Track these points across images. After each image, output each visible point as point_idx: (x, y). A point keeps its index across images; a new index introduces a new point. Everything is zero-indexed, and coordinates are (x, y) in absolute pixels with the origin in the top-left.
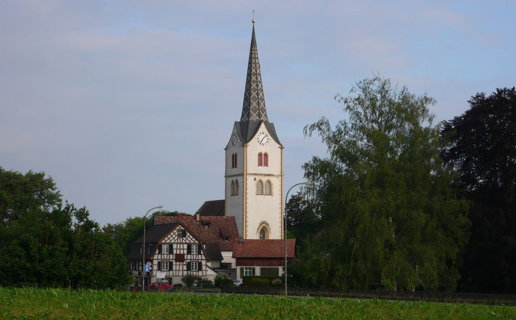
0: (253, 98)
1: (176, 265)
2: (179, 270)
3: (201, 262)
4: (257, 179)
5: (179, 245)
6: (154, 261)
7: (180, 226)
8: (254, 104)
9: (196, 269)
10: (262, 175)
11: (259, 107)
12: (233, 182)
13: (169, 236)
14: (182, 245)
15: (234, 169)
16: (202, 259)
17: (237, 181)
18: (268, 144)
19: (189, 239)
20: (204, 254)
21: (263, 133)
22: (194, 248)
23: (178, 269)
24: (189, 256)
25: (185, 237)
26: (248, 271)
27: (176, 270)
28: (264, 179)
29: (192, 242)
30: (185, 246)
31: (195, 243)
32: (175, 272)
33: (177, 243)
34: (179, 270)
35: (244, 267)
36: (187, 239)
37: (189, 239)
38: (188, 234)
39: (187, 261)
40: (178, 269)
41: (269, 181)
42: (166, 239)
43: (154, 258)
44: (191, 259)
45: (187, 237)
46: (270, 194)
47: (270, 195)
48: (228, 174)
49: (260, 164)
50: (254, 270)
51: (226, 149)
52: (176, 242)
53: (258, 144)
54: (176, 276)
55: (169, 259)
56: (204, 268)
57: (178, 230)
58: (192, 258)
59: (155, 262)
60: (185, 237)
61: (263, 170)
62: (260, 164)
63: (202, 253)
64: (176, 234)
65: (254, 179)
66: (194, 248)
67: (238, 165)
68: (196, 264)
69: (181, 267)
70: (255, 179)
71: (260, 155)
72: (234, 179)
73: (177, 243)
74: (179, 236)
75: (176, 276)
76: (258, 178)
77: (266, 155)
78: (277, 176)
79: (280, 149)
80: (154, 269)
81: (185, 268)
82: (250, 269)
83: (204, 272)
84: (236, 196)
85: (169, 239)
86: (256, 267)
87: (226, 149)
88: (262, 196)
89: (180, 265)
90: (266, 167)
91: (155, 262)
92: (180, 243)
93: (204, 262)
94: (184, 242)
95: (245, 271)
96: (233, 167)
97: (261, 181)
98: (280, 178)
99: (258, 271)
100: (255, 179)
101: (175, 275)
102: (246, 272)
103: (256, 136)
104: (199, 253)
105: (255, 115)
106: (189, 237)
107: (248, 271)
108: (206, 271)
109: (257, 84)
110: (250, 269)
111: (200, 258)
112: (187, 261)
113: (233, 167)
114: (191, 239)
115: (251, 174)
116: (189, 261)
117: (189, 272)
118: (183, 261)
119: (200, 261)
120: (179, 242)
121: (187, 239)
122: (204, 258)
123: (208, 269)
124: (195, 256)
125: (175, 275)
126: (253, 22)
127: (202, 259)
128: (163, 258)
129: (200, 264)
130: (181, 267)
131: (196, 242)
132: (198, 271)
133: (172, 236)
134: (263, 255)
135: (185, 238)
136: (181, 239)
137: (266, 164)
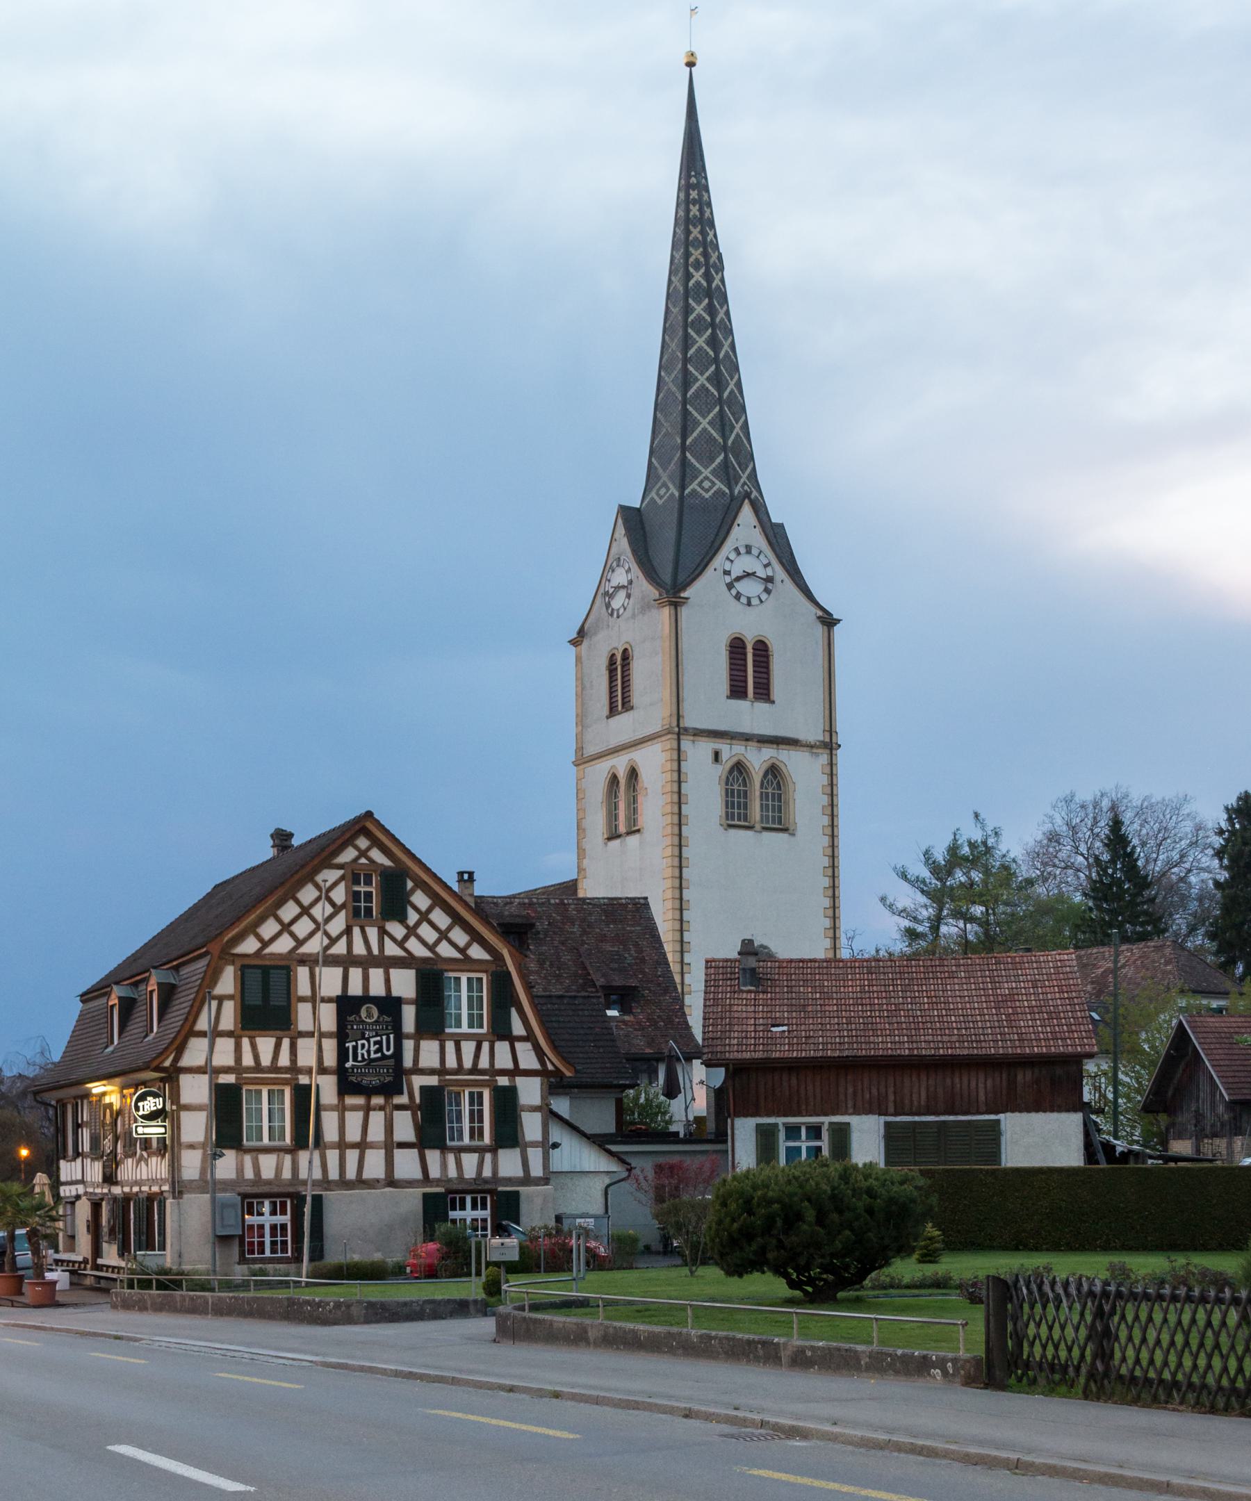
0: (696, 394)
1: (342, 1109)
2: (363, 1146)
3: (512, 1092)
4: (725, 756)
5: (356, 974)
6: (185, 1079)
7: (363, 843)
8: (704, 423)
9: (476, 1133)
10: (747, 738)
11: (725, 438)
12: (614, 779)
13: (289, 911)
14: (376, 975)
15: (624, 720)
16: (516, 1072)
17: (633, 774)
18: (771, 601)
19: (426, 931)
20: (530, 1037)
21: (749, 549)
22: (465, 1000)
23: (353, 1135)
24: (429, 1053)
25: (402, 919)
26: (804, 1145)
27: (342, 1145)
28: (758, 759)
29: (445, 950)
30: (404, 984)
31: (466, 962)
32: (333, 1156)
33: (347, 961)
34: (363, 1146)
35: (780, 1121)
36: (412, 931)
37: (426, 931)
38: (421, 900)
39: (418, 1081)
40: (353, 1135)
41: (774, 772)
42: (269, 928)
43: (185, 1062)
44: (442, 1071)
45: (413, 917)
46: (778, 822)
47: (785, 830)
48: (591, 750)
49: (737, 691)
50: (841, 1136)
51: (575, 643)
52: (340, 948)
53: (728, 596)
54: (344, 1183)
55: (294, 1069)
56: (532, 1126)
57: (354, 875)
58: (451, 1062)
59: (195, 1090)
60: (402, 919)
61: (749, 716)
62: (737, 691)
63: (518, 1028)
64: (339, 895)
65: (710, 757)
66: (465, 1000)
67: (636, 699)
68: (476, 1099)
69: (377, 1119)
70: (717, 756)
71: (736, 647)
72: (620, 764)
73: (347, 961)
74: (358, 912)
75: (344, 1183)
76: (731, 752)
77: (762, 649)
78: (811, 746)
79: (819, 630)
80: (186, 1137)
81: (405, 1127)
82: (815, 1132)
83: (535, 1156)
84: (633, 840)
85: (286, 928)
86: (855, 1121)
87: (575, 643)
88: (750, 833)
89: (367, 1109)
90: (762, 706)
91: (195, 1090)
92: (367, 962)
93: (530, 1091)
94: (392, 950)
95: (783, 1144)
96: (613, 711)
97: (739, 768)
98: (824, 758)
99: (867, 1141)
100: (717, 756)
101: (334, 1174)
102: (793, 1153)
103: (719, 562)
104: (501, 1031)
105: (706, 472)
106: (424, 917)
107: (804, 1145)
108: (549, 1146)
109: (714, 335)
110: (815, 1132)
111: (503, 1059)
112: (418, 1081)
113: (613, 711)
114: (443, 935)
115: (699, 733)
116: (433, 1081)
117: (433, 1156)
118: (391, 1088)
119: (503, 1081)
120: (359, 949)
121: (412, 931)
122: (528, 1059)
123: (557, 1134)
124: (468, 1048)
125: (334, 1174)
126: (691, 64)
127: (516, 1072)
128: (248, 1060)
129: (506, 1103)
130: (377, 1119)
131: (476, 952)
132: (493, 1149)
133: (305, 911)
134: (884, 1044)
135: (397, 930)
136: (372, 933)
137: (764, 692)
